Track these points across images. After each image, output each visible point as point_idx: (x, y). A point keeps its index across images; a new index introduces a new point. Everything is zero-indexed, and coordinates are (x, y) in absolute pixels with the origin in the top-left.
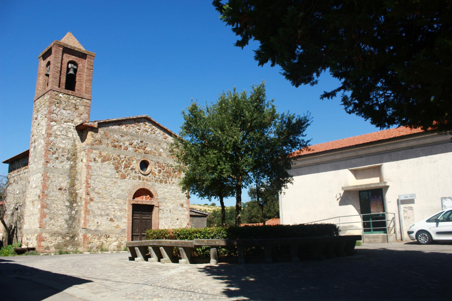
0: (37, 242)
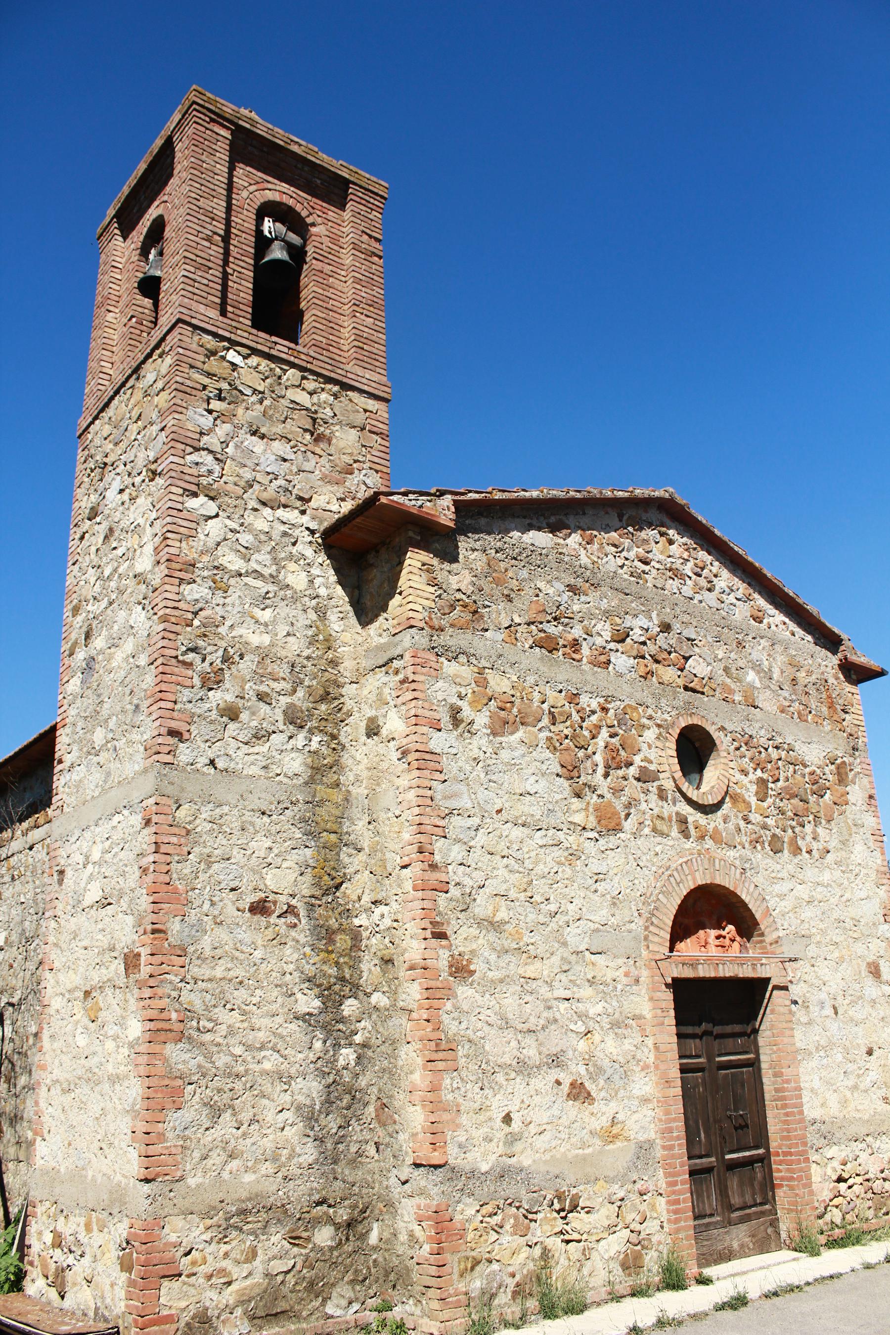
0: (131, 1283)
